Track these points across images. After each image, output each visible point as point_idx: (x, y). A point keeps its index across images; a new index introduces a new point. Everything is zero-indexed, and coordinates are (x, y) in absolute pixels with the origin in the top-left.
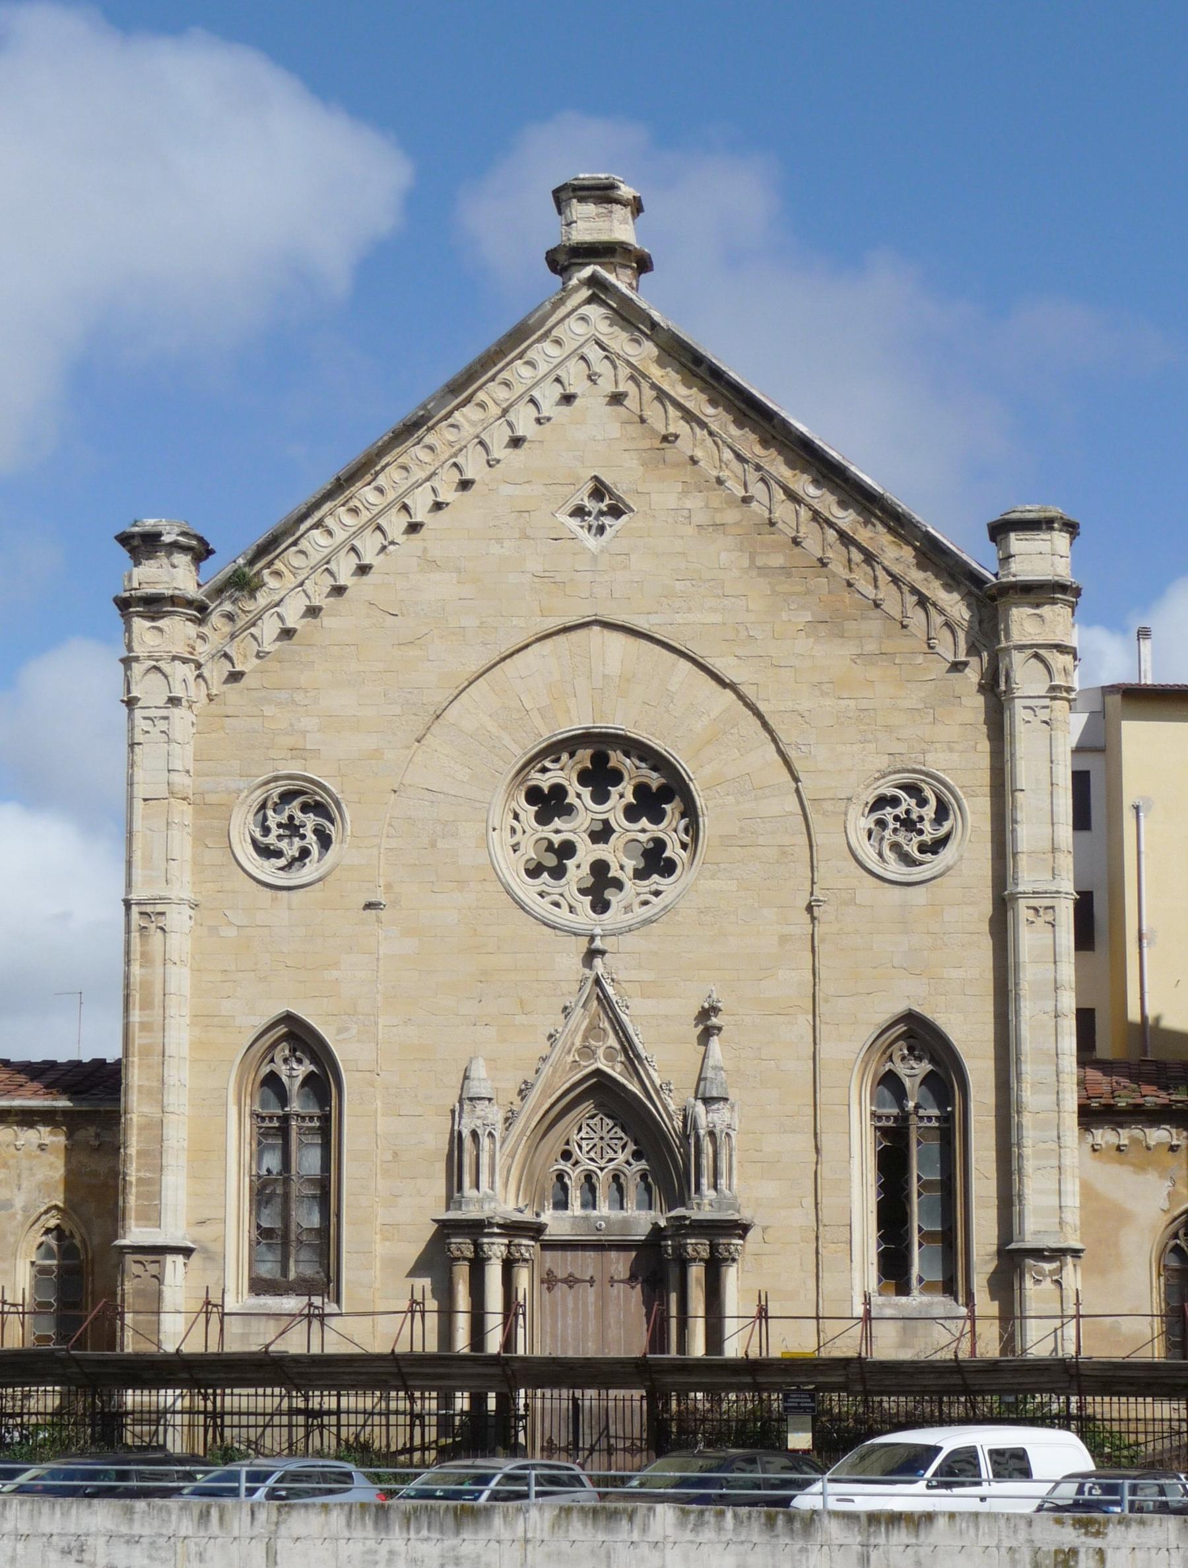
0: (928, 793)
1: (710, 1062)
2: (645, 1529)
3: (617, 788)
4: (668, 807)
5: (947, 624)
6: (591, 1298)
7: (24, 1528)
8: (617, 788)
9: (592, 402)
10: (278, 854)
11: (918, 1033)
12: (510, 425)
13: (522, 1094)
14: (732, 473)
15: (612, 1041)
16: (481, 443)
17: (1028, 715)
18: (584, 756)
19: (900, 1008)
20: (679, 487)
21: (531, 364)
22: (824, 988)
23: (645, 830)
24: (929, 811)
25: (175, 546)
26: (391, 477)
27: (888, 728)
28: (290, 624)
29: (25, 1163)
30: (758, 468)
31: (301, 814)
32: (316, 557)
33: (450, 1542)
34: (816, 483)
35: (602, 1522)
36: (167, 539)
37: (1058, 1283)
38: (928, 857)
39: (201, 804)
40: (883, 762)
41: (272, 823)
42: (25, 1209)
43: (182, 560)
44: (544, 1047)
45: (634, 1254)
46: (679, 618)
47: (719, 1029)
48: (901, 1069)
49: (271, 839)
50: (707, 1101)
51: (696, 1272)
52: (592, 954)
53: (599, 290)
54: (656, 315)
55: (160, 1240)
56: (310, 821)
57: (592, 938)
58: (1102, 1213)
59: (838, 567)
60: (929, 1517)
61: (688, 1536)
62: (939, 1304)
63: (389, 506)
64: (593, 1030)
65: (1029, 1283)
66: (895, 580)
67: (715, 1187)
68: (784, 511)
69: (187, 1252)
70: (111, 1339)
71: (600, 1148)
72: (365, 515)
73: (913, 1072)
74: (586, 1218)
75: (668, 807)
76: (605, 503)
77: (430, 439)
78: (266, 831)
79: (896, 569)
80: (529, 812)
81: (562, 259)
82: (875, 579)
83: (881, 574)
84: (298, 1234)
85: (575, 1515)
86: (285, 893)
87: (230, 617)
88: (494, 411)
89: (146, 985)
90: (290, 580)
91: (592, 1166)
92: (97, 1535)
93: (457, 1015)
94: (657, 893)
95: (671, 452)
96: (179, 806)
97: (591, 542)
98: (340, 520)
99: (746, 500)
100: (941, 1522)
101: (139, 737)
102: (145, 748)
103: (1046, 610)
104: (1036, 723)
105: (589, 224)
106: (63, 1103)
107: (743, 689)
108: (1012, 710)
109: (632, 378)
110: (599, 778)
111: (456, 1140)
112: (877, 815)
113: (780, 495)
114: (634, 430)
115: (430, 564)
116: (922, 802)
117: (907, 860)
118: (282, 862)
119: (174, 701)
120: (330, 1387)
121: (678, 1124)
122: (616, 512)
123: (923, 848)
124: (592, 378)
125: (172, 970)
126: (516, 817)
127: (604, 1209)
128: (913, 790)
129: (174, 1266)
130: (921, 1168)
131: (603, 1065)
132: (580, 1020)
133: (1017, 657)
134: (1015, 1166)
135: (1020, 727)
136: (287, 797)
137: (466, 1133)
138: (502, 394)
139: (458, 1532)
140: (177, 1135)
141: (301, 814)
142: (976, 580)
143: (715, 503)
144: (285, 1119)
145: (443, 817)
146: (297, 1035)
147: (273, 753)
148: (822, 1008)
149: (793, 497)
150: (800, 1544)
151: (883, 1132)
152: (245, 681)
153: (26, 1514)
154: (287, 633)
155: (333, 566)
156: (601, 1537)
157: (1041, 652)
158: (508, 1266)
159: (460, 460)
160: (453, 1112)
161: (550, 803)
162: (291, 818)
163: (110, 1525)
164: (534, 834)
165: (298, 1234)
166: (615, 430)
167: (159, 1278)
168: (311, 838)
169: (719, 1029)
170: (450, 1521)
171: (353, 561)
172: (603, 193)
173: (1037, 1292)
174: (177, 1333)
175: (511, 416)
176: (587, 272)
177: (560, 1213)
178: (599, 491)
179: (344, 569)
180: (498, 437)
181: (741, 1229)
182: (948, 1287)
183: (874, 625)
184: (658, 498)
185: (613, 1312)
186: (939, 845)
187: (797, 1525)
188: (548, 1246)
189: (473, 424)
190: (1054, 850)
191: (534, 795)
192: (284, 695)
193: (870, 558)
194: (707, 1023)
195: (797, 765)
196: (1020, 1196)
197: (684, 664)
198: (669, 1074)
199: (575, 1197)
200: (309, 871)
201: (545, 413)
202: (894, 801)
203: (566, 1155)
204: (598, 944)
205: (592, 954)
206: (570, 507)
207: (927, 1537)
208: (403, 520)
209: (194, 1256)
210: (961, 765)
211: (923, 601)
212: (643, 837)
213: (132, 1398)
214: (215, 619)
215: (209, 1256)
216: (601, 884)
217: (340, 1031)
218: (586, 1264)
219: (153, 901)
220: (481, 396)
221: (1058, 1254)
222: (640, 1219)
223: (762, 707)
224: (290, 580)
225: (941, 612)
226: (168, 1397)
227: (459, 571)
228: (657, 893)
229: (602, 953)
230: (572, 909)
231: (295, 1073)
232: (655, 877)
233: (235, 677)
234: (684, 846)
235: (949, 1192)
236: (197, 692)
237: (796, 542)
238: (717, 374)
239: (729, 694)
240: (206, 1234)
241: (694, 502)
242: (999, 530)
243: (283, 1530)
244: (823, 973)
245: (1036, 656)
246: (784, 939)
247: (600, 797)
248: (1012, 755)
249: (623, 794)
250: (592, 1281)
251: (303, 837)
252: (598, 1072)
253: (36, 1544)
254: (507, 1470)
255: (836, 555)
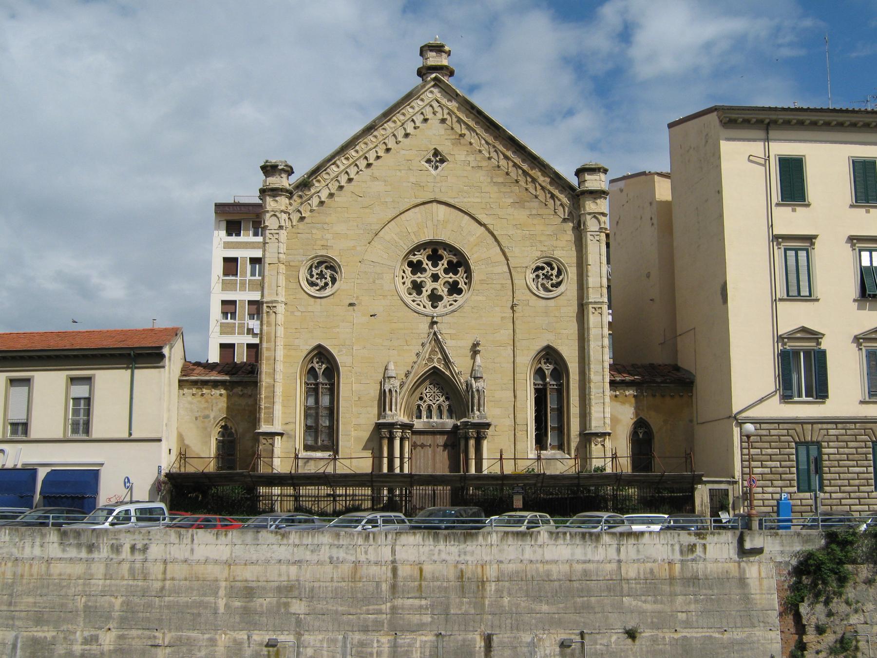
0: (555, 265)
1: (477, 364)
2: (536, 540)
3: (441, 264)
4: (460, 269)
5: (561, 205)
6: (430, 452)
7: (297, 542)
8: (441, 264)
9: (434, 121)
10: (317, 285)
11: (550, 354)
12: (405, 129)
13: (407, 376)
14: (485, 148)
15: (440, 356)
16: (394, 135)
17: (592, 238)
18: (429, 251)
19: (545, 344)
20: (465, 153)
21: (413, 108)
22: (519, 336)
23: (451, 278)
24: (555, 272)
25: (283, 170)
26: (361, 147)
27: (541, 242)
28: (323, 199)
29: (214, 401)
30: (494, 147)
31: (325, 270)
32: (333, 175)
33: (462, 546)
34: (514, 152)
35: (520, 538)
36: (280, 167)
37: (603, 445)
38: (554, 289)
39: (288, 266)
40: (538, 254)
41: (314, 273)
42: (214, 418)
43: (284, 176)
44: (415, 359)
45: (446, 437)
46: (465, 200)
47: (479, 351)
48: (544, 367)
49: (314, 279)
50: (476, 378)
51: (472, 442)
52: (433, 323)
53: (437, 82)
54: (458, 92)
55: (273, 431)
56: (328, 273)
57: (433, 317)
58: (615, 420)
59: (522, 183)
60: (642, 533)
61: (553, 542)
62: (558, 454)
63: (360, 157)
64: (433, 352)
65: (593, 445)
66: (543, 188)
67: (479, 410)
68: (503, 163)
69: (281, 434)
70: (255, 468)
71: (433, 397)
72: (351, 160)
73: (548, 368)
74: (428, 422)
75: (460, 269)
76: (438, 158)
77: (375, 133)
78: (312, 276)
79: (543, 184)
80: (408, 270)
81: (424, 71)
82: (536, 188)
83: (537, 185)
84: (322, 429)
85: (510, 535)
86: (319, 300)
87: (301, 197)
88: (399, 124)
89: (268, 334)
90: (323, 184)
91: (431, 403)
92: (325, 545)
93: (381, 346)
94: (456, 301)
95: (462, 141)
96: (282, 267)
97: (433, 172)
98: (342, 162)
99: (490, 158)
100: (647, 535)
101: (268, 240)
102: (270, 244)
103: (598, 201)
104: (595, 241)
105: (433, 59)
106: (227, 378)
107: (491, 227)
108: (586, 236)
109: (449, 113)
110: (435, 258)
111: (383, 394)
112: (536, 273)
113: (502, 157)
114: (449, 132)
115: (375, 179)
116: (552, 269)
117: (546, 290)
118: (318, 288)
119: (281, 227)
120: (342, 486)
121: (464, 387)
122: (442, 161)
123: (552, 286)
124: (434, 113)
125: (279, 328)
126: (404, 272)
127: (435, 419)
128: (549, 264)
129: (278, 439)
130: (551, 403)
131: (436, 365)
132: (428, 348)
133: (588, 217)
134: (587, 402)
135: (589, 242)
136: (320, 263)
137: (387, 390)
138: (402, 118)
139: (465, 542)
140: (279, 390)
141: (325, 270)
142: (572, 188)
143: (478, 159)
144: (317, 384)
145: (376, 270)
146: (321, 353)
147: (315, 247)
148: (517, 344)
149: (506, 157)
150: (594, 544)
151: (537, 390)
152: (306, 221)
153: (298, 536)
154: (322, 203)
155: (339, 178)
156: (520, 543)
157: (599, 217)
158: (402, 440)
159: (386, 141)
160: (381, 383)
161: (416, 267)
162: (322, 271)
163: (331, 541)
164: (410, 277)
165: (322, 429)
166: (442, 132)
167: (272, 445)
168: (329, 279)
169: (479, 351)
170: (462, 538)
171: (346, 177)
172: (438, 49)
173: (596, 449)
174: (280, 465)
175: (405, 126)
176: (433, 76)
177: (419, 420)
178: (436, 153)
179: (343, 179)
180: (400, 134)
181: (488, 425)
182: (560, 447)
183: (535, 204)
184: (458, 156)
185: (438, 458)
186: (558, 284)
187: (593, 537)
188: (415, 433)
189: (391, 128)
190: (601, 287)
191: (410, 264)
192: (320, 225)
193: (534, 180)
194: (475, 350)
195: (508, 254)
196: (590, 413)
197: (467, 217)
198: (461, 365)
199: (424, 414)
200: (328, 291)
201: (417, 125)
202: (543, 268)
203: (421, 399)
204: (435, 319)
205: (433, 323)
206: (425, 159)
207: (752, 541)
208: (365, 162)
209: (284, 437)
210: (567, 255)
211: (553, 196)
212: (451, 280)
213: (262, 490)
214: (295, 197)
215: (289, 436)
216: (435, 298)
217: (339, 352)
218: (428, 440)
219: (272, 302)
220: (394, 118)
221: (604, 435)
222: (449, 422)
223: (495, 233)
224: (323, 184)
225: (559, 200)
226: (276, 491)
227: (385, 181)
228: (456, 301)
229: (436, 323)
230: (424, 307)
231: (320, 368)
232: (455, 295)
233: (302, 219)
234: (466, 284)
235: (561, 412)
236: (288, 224)
237: (507, 174)
238: (480, 113)
239: (483, 229)
240: (289, 428)
241: (471, 158)
242: (579, 172)
243: (398, 542)
244: (517, 331)
245: (595, 217)
246: (503, 318)
247: (435, 265)
248: (586, 252)
249: (443, 264)
250: (430, 446)
251: (326, 278)
252: (435, 367)
253: (302, 548)
254: (369, 517)
255: (522, 179)
